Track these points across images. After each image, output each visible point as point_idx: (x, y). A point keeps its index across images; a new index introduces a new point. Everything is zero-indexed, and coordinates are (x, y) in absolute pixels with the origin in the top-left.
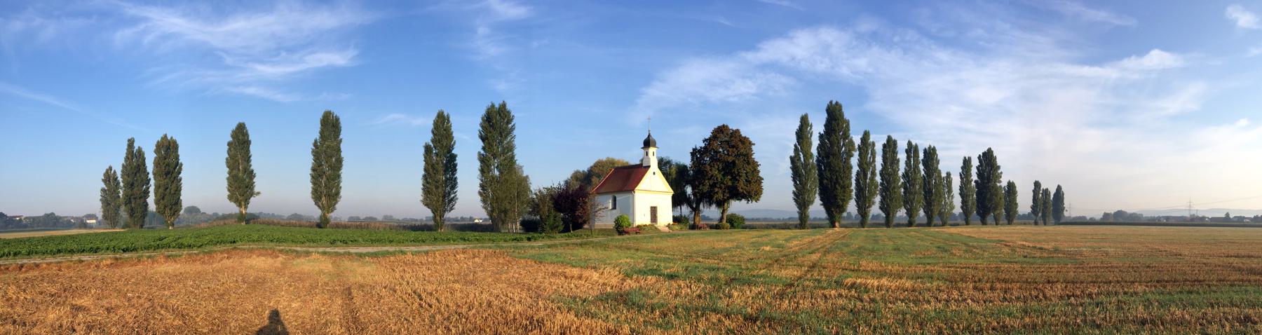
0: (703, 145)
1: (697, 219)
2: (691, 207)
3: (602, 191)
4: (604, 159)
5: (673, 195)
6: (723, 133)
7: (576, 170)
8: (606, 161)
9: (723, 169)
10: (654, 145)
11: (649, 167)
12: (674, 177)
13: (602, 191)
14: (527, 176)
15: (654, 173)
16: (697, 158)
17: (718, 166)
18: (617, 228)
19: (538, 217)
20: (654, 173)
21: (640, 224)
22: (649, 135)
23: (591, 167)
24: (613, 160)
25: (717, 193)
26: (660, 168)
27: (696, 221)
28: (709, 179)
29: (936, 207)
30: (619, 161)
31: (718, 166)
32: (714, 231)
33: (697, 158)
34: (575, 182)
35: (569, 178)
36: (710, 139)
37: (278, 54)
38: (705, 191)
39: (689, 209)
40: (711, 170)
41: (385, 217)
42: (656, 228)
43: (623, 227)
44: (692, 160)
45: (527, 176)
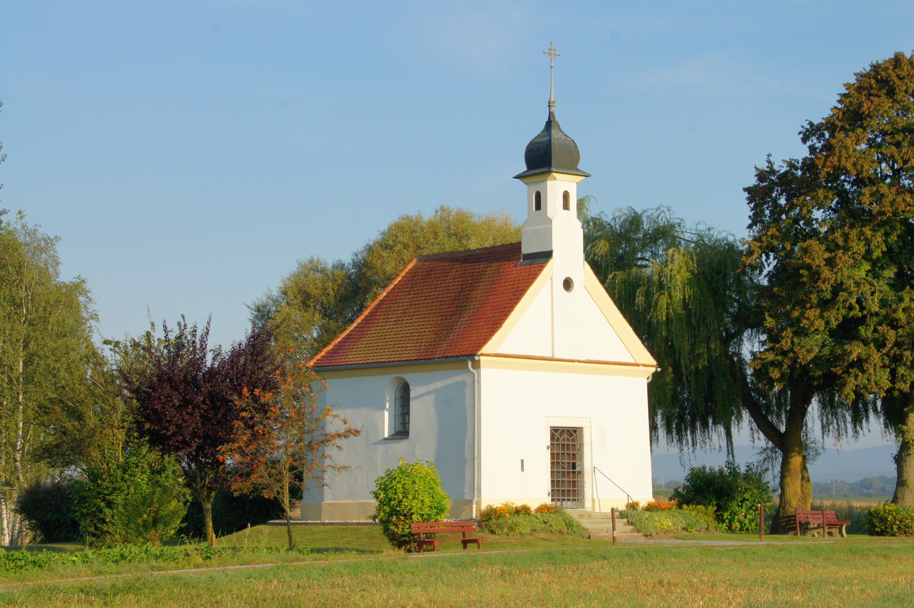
0: (801, 152)
1: (794, 486)
2: (769, 430)
3: (354, 357)
4: (428, 214)
5: (655, 375)
6: (891, 93)
7: (305, 259)
8: (431, 224)
9: (891, 255)
10: (571, 166)
11: (547, 255)
12: (678, 295)
13: (354, 357)
14: (77, 287)
15: (568, 284)
16: (777, 211)
17: (868, 242)
18: (385, 523)
19: (74, 473)
20: (568, 284)
21: (497, 504)
22: (549, 124)
23: (370, 249)
24: (462, 218)
25: (860, 364)
26: (599, 267)
27: (789, 491)
28: (825, 304)
29: (852, 379)
30: (489, 224)
31: (868, 242)
32: (862, 540)
33: (777, 211)
34: (297, 315)
35: (275, 293)
36: (830, 125)
37: (164, 458)
38: (805, 357)
39: (762, 441)
40: (830, 263)
41: (459, 213)
42: (570, 524)
43: (408, 516)
44: (756, 219)
45: (77, 287)
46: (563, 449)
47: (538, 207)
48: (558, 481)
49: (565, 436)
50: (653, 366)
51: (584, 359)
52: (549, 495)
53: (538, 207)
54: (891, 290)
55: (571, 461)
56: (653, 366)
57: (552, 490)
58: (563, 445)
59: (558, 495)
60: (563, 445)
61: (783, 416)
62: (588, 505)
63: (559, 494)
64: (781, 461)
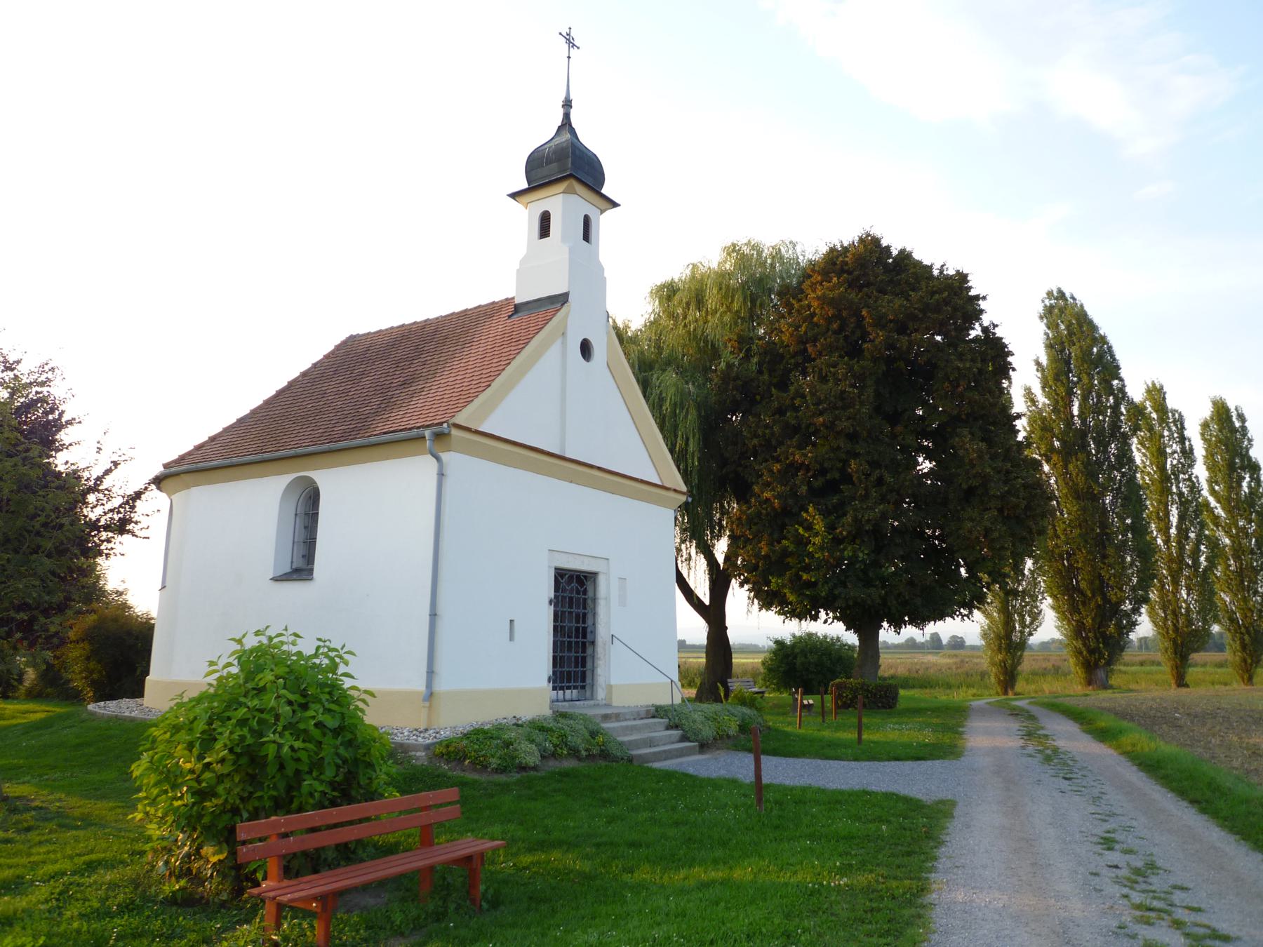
0: (1136, 392)
46: (570, 607)
47: (586, 237)
48: (563, 613)
49: (574, 584)
50: (683, 493)
51: (609, 374)
52: (549, 682)
53: (586, 237)
54: (883, 719)
55: (580, 654)
56: (683, 493)
57: (554, 672)
58: (571, 599)
59: (569, 681)
60: (571, 599)
61: (677, 449)
62: (601, 694)
63: (569, 629)
64: (753, 769)
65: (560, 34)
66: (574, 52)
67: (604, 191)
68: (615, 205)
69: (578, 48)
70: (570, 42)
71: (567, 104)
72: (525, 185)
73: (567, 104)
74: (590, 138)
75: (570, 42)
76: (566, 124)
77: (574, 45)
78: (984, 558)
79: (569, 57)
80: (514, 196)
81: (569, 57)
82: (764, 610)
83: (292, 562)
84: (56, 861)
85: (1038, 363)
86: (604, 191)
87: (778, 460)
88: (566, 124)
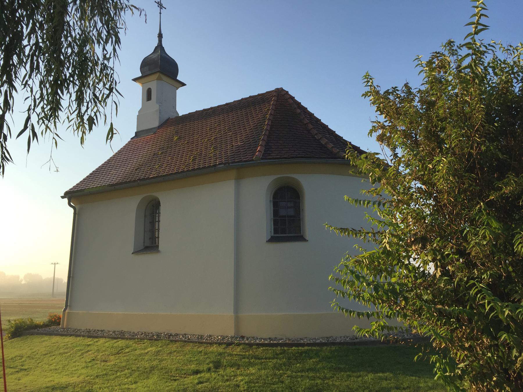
65: (165, 8)
66: (163, 10)
67: (178, 78)
68: (185, 85)
69: (155, 2)
70: (160, 5)
71: (160, 36)
72: (140, 75)
73: (160, 36)
74: (171, 51)
75: (160, 5)
76: (160, 47)
77: (158, 3)
78: (496, 390)
79: (160, 13)
80: (135, 80)
81: (160, 13)
82: (66, 200)
83: (144, 242)
84: (177, 377)
85: (16, 91)
86: (178, 78)
87: (71, 75)
88: (160, 47)
